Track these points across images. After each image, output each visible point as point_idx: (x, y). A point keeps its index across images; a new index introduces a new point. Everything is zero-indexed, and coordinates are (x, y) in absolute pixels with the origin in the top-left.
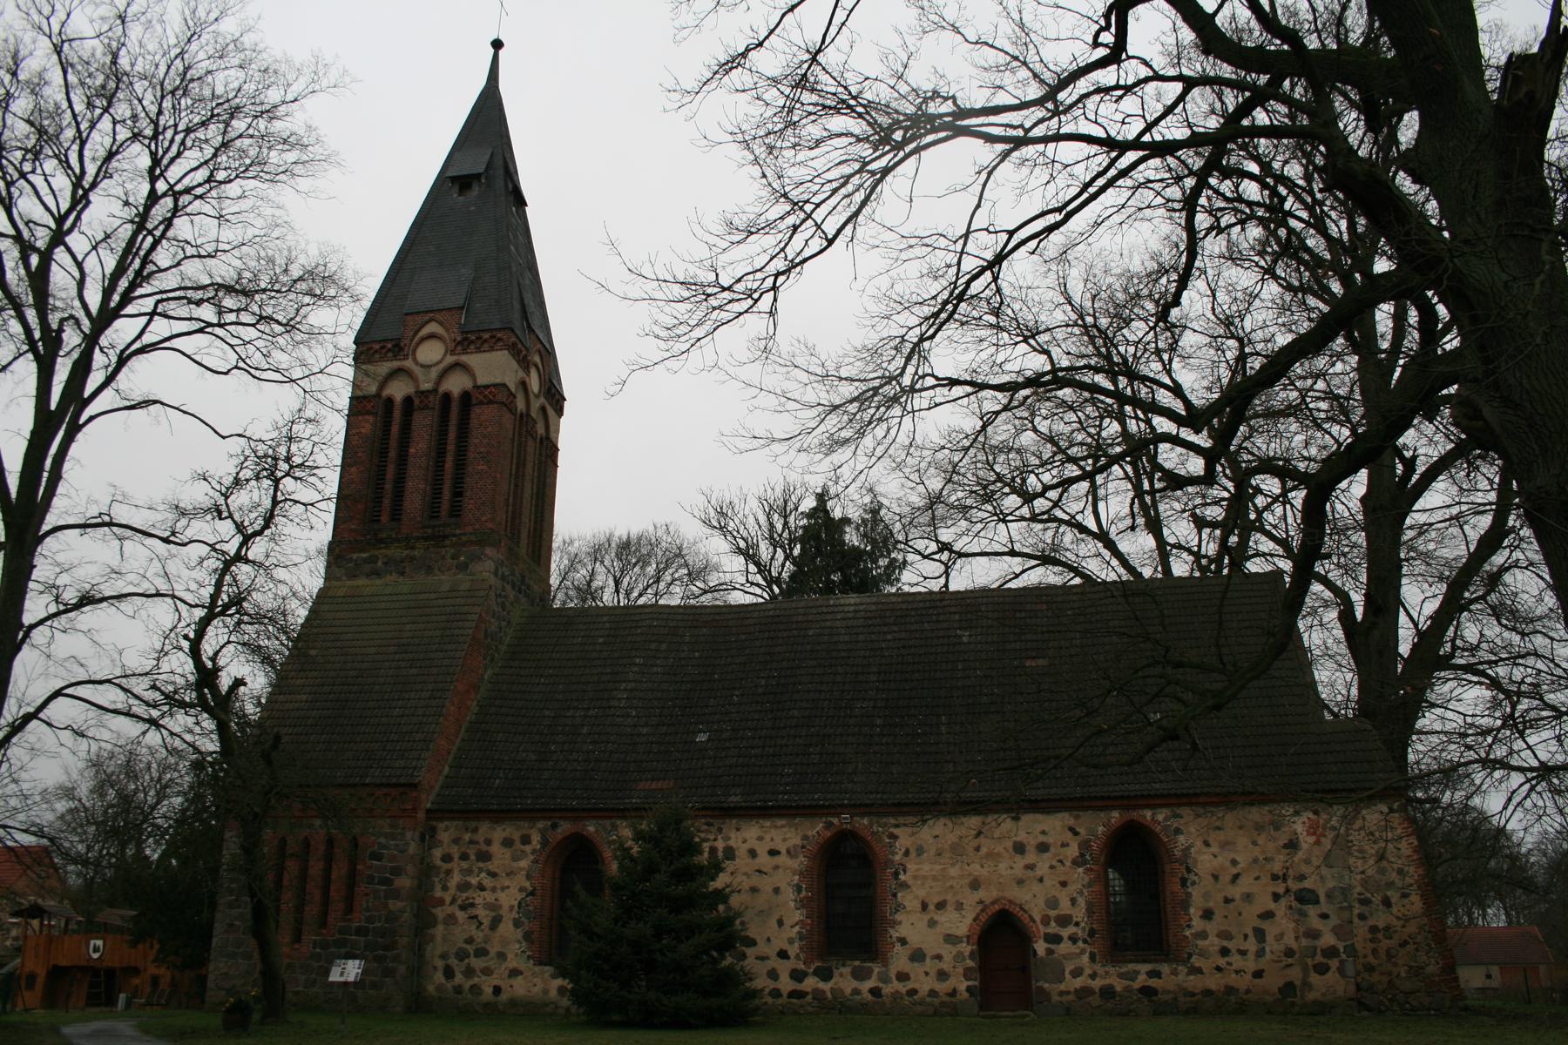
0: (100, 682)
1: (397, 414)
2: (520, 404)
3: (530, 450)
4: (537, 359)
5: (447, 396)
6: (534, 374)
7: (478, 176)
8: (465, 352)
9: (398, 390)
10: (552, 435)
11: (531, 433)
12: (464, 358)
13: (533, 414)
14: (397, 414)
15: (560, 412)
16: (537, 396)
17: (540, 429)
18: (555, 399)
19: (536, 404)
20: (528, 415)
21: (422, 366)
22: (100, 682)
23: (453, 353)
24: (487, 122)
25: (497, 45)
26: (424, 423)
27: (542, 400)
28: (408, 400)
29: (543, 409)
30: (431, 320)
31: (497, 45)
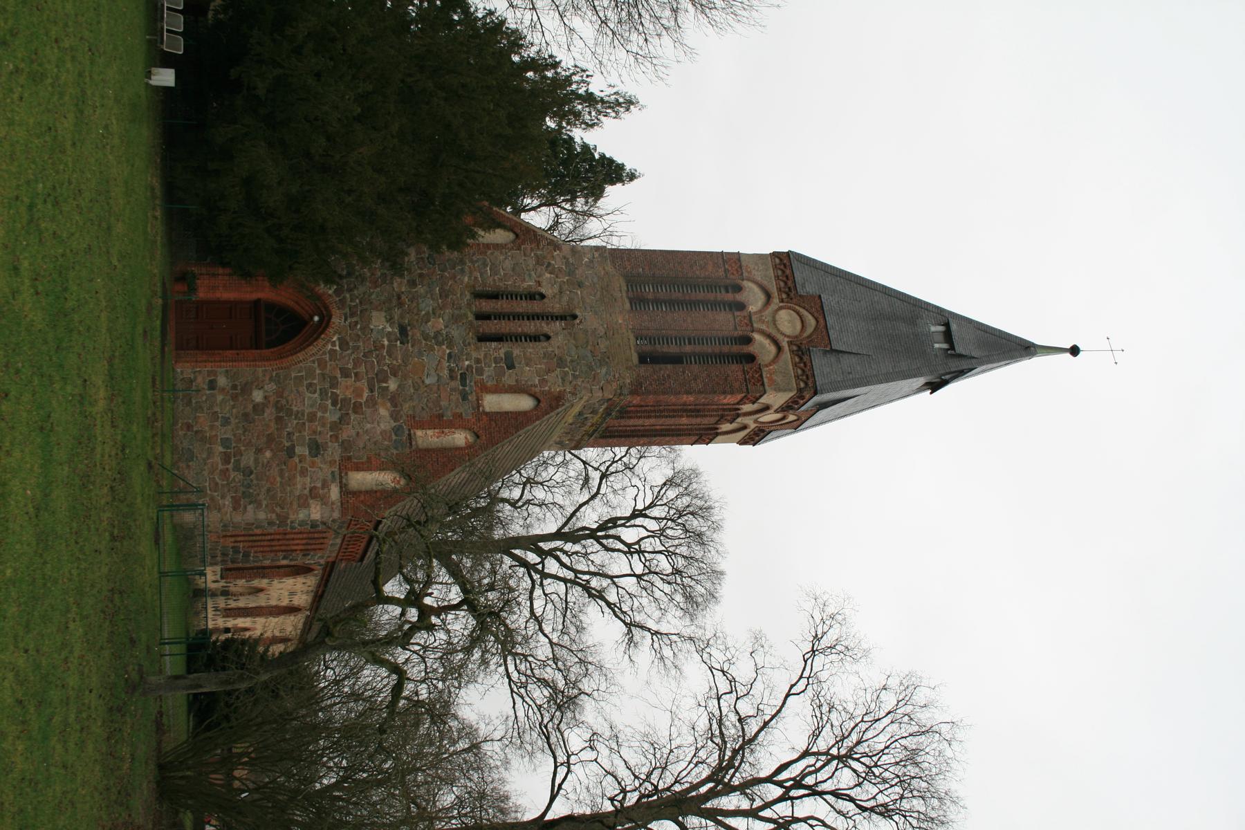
0: (784, 703)
1: (729, 297)
2: (747, 407)
3: (706, 421)
4: (791, 418)
5: (738, 289)
6: (779, 416)
7: (952, 347)
8: (792, 352)
9: (754, 299)
10: (719, 438)
11: (722, 418)
12: (787, 355)
13: (739, 420)
14: (729, 297)
15: (743, 442)
16: (756, 421)
17: (726, 427)
18: (755, 437)
19: (749, 421)
20: (738, 416)
21: (774, 317)
22: (784, 703)
23: (790, 343)
24: (1009, 348)
25: (1075, 351)
26: (724, 322)
27: (753, 426)
28: (751, 358)
29: (745, 427)
30: (816, 319)
31: (1075, 351)
